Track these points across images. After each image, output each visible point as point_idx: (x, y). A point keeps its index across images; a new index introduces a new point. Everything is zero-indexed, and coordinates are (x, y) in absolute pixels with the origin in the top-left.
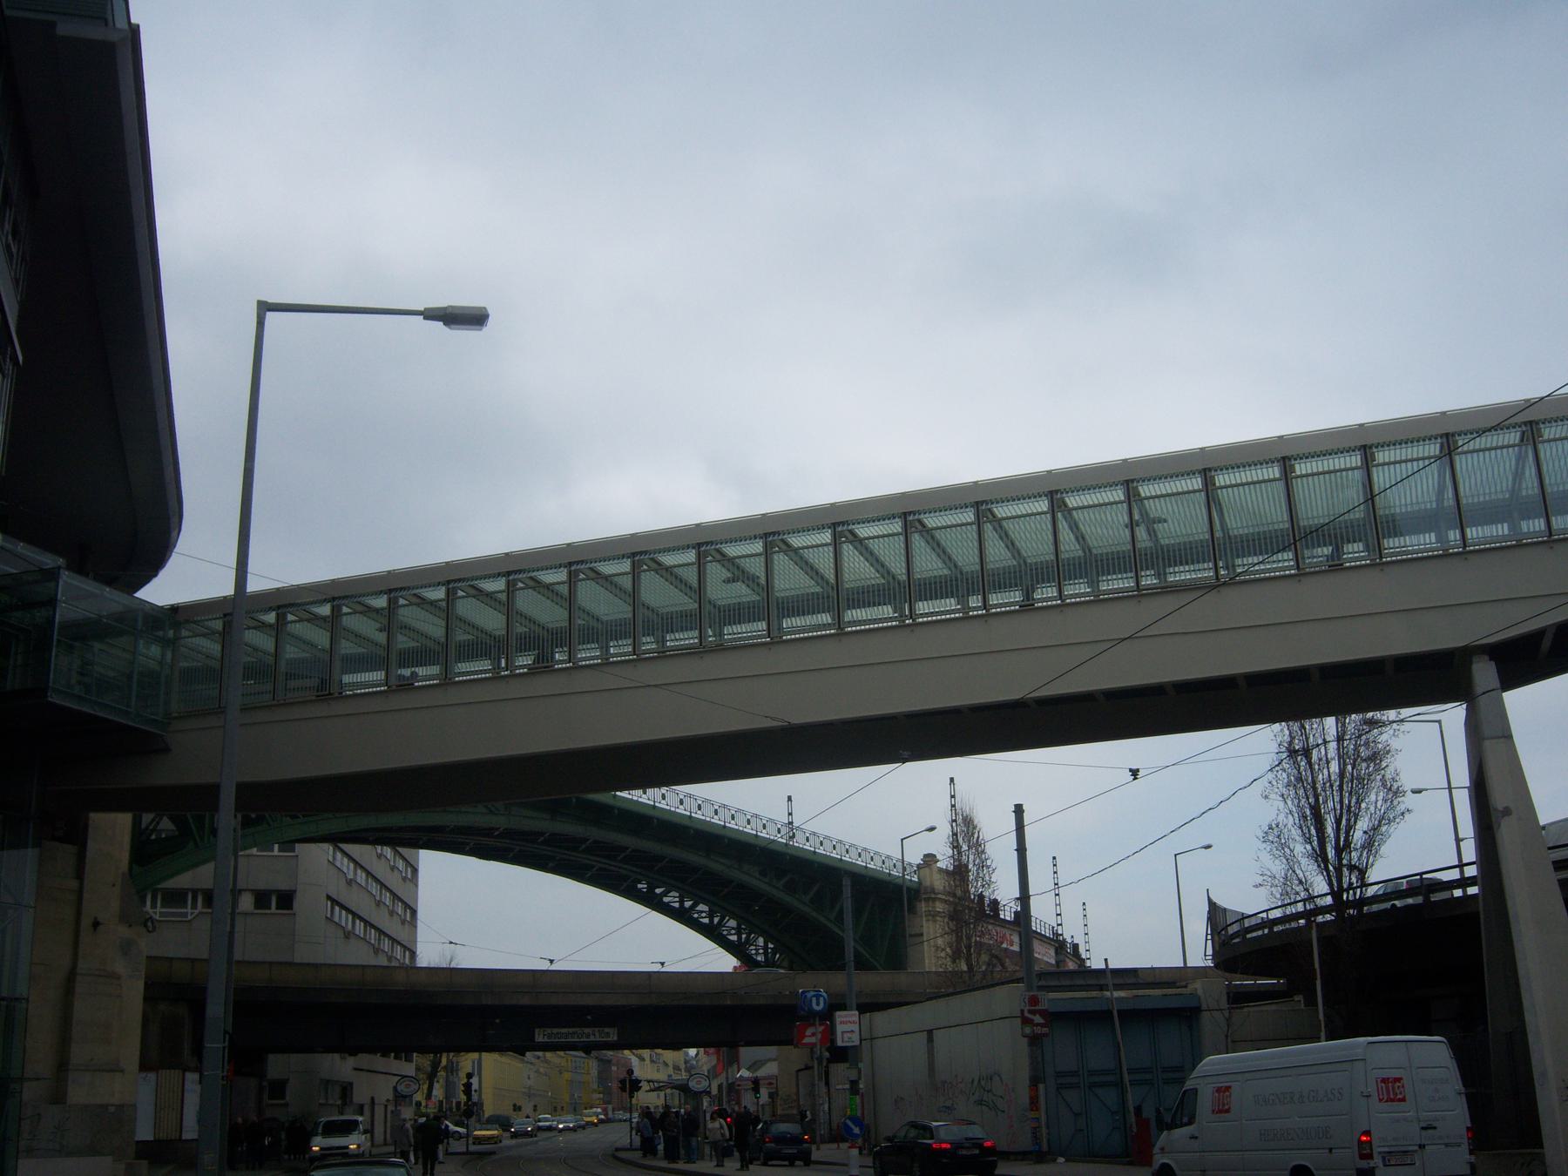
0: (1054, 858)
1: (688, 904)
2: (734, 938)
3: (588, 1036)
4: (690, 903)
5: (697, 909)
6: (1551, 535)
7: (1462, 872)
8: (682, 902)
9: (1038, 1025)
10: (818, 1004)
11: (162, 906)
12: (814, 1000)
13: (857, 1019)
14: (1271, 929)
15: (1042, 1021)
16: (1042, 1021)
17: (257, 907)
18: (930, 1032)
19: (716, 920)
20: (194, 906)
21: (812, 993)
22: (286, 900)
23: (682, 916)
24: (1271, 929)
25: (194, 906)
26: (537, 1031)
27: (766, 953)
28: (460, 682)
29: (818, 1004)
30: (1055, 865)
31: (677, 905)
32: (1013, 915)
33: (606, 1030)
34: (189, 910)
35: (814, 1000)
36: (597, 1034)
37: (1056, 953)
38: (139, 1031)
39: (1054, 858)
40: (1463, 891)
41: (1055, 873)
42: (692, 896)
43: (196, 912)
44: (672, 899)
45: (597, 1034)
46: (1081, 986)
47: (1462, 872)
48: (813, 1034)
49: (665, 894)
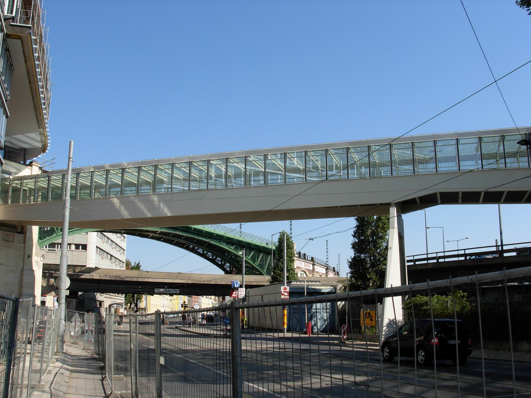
0: (327, 241)
1: (205, 252)
2: (220, 263)
3: (170, 291)
4: (206, 252)
5: (208, 254)
6: (437, 172)
7: (427, 256)
8: (203, 252)
9: (286, 295)
10: (237, 285)
11: (49, 248)
12: (236, 284)
13: (245, 290)
14: (415, 263)
15: (287, 294)
16: (287, 294)
17: (76, 249)
18: (262, 296)
19: (214, 257)
20: (58, 248)
21: (235, 282)
22: (84, 247)
23: (203, 256)
24: (438, 261)
25: (58, 248)
26: (155, 289)
27: (230, 268)
28: (141, 195)
29: (237, 285)
30: (327, 243)
31: (202, 253)
32: (311, 258)
33: (176, 290)
34: (56, 249)
35: (236, 284)
36: (173, 291)
37: (326, 270)
38: (64, 312)
39: (327, 241)
40: (438, 261)
41: (327, 245)
42: (206, 250)
43: (58, 249)
44: (200, 251)
45: (173, 291)
46: (318, 285)
47: (427, 256)
48: (236, 294)
49: (198, 249)
